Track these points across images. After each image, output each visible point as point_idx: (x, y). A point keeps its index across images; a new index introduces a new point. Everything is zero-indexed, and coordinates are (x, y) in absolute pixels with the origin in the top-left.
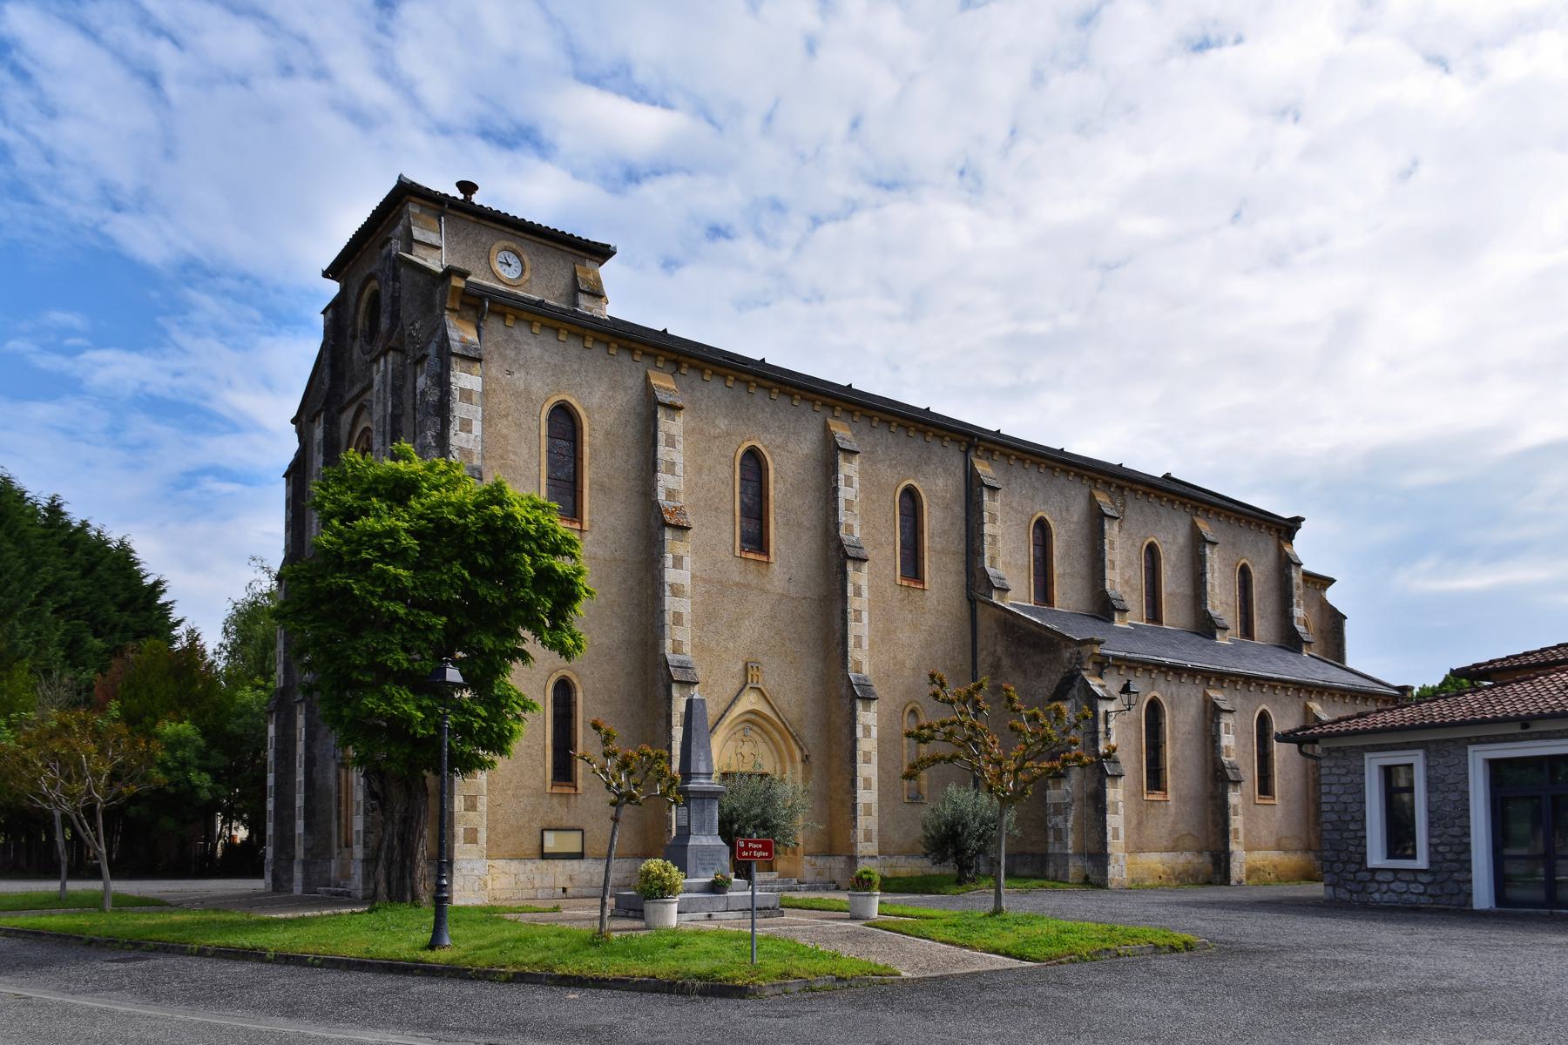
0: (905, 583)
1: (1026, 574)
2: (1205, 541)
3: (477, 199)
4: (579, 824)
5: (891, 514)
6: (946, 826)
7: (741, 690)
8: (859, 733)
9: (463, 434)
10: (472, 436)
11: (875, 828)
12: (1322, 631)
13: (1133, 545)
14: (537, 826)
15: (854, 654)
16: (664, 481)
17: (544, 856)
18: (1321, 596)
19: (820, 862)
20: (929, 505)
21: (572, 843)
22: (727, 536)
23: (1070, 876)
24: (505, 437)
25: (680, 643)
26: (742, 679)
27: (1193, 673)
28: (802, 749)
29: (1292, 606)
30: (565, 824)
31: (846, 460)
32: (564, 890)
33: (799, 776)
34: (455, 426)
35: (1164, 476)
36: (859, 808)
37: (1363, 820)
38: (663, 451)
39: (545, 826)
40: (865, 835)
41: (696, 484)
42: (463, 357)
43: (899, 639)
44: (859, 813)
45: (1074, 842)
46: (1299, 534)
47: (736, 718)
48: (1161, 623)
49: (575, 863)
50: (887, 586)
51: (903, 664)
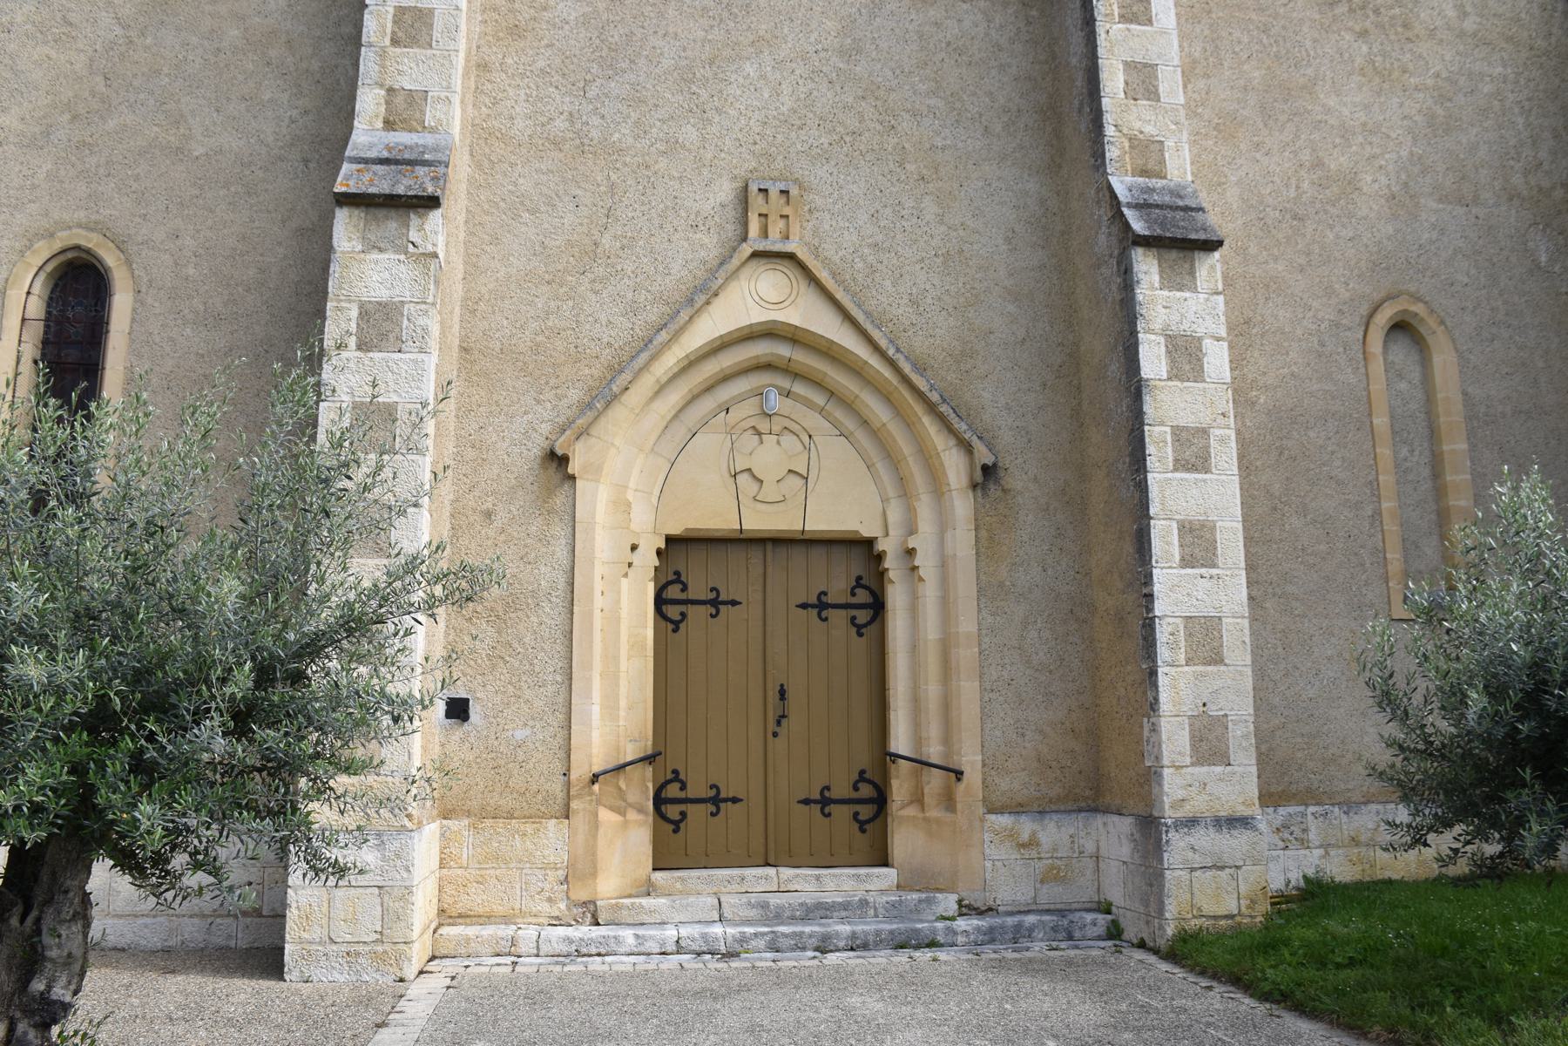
6: (1495, 692)
8: (1153, 361)
11: (1239, 708)
19: (1054, 833)
25: (417, 99)
26: (731, 230)
28: (967, 447)
33: (963, 541)
36: (1162, 634)
40: (1197, 739)
43: (1328, 110)
44: (1163, 653)
47: (692, 363)
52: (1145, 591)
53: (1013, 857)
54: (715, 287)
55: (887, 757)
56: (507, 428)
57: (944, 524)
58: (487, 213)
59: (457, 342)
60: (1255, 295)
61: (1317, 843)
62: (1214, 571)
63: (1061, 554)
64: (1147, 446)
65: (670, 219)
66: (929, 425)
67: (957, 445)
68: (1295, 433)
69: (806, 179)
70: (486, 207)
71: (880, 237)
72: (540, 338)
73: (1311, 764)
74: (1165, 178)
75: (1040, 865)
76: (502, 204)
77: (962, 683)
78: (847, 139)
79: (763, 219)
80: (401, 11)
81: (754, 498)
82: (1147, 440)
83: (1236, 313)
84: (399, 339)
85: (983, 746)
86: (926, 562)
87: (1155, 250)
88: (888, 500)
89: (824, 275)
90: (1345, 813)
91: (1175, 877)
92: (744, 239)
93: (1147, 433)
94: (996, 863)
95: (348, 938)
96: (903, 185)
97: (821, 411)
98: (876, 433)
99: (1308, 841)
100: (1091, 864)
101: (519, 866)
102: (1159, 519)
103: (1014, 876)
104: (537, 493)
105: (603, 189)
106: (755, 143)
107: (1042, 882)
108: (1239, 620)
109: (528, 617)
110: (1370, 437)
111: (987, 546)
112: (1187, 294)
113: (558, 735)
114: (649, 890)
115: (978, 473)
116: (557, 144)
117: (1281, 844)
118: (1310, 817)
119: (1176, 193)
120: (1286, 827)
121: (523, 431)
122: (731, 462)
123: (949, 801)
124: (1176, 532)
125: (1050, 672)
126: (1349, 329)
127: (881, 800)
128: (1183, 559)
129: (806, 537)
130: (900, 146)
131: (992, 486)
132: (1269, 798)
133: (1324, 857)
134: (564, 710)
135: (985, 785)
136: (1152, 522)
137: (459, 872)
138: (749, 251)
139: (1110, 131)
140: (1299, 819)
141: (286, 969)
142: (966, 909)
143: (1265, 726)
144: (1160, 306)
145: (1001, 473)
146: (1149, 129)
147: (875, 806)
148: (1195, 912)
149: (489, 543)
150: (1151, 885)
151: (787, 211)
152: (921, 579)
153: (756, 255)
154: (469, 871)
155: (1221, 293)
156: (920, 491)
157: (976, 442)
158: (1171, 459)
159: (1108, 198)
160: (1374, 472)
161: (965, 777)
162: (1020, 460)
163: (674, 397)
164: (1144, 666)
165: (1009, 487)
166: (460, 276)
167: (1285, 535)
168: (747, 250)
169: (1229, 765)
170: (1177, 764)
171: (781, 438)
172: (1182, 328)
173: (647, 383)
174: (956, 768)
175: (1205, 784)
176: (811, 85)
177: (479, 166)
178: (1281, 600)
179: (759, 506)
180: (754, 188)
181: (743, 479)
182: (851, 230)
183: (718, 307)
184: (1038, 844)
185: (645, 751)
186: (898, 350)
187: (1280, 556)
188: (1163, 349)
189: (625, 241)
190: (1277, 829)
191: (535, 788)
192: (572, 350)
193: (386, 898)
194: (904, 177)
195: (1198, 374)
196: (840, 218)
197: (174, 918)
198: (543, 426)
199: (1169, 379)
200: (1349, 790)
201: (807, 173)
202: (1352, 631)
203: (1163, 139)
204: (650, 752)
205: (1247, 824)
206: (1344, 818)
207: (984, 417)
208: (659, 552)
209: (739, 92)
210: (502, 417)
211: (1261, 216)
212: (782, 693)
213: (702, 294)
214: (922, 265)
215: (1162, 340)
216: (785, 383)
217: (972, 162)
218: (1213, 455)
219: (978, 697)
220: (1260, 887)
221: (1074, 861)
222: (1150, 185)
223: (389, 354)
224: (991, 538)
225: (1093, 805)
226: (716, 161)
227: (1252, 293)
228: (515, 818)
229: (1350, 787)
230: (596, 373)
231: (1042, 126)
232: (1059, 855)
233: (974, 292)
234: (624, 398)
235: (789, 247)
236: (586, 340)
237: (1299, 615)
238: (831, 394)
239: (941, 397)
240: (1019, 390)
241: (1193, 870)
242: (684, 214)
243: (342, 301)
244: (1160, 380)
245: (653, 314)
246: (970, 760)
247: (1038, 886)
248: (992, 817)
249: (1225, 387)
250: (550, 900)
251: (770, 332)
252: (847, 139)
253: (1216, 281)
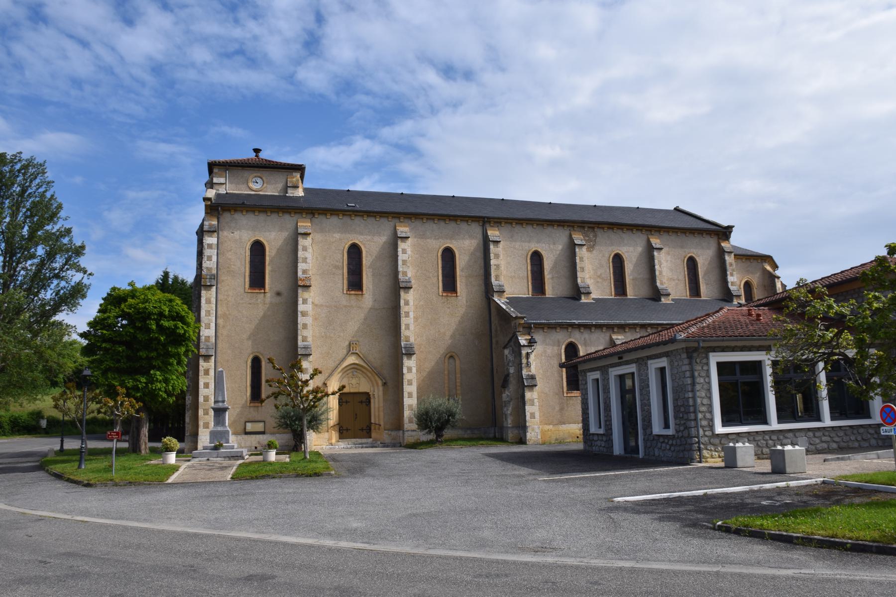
0: (444, 294)
1: (525, 281)
2: (654, 248)
3: (262, 155)
4: (263, 419)
5: (436, 262)
7: (347, 354)
8: (405, 370)
9: (208, 262)
10: (212, 262)
12: (765, 286)
13: (603, 256)
14: (243, 420)
15: (404, 332)
16: (301, 266)
17: (246, 433)
18: (763, 266)
19: (394, 433)
20: (460, 255)
21: (259, 427)
22: (340, 285)
23: (509, 438)
24: (230, 259)
25: (306, 337)
27: (599, 327)
29: (727, 276)
30: (256, 419)
31: (402, 242)
32: (256, 448)
33: (381, 393)
34: (205, 259)
35: (675, 209)
36: (405, 407)
37: (650, 406)
38: (301, 254)
39: (247, 420)
41: (323, 264)
42: (208, 231)
45: (512, 421)
46: (733, 235)
48: (627, 295)
49: (261, 436)
50: (434, 297)
80: (303, 324)
86: (376, 396)
91: (406, 437)
111: (384, 394)
114: (339, 442)
116: (323, 337)
123: (379, 429)
127: (370, 429)
142: (381, 443)
147: (580, 446)
163: (341, 374)
173: (337, 372)
195: (411, 372)
212: (356, 415)
213: (344, 359)
238: (363, 372)
245: (338, 362)
246: (382, 423)
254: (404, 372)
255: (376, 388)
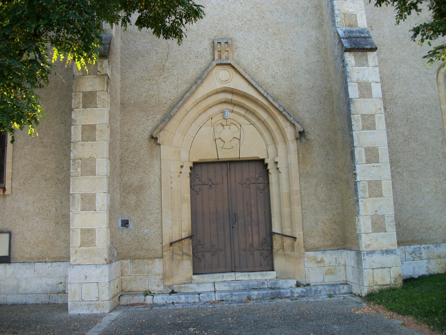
8: (353, 91)
28: (294, 125)
33: (293, 158)
36: (360, 187)
40: (374, 224)
44: (360, 194)
51: (78, 61)
52: (354, 172)
53: (315, 266)
54: (204, 77)
55: (272, 234)
56: (137, 129)
57: (287, 153)
58: (127, 58)
59: (119, 102)
60: (396, 65)
61: (425, 258)
62: (378, 164)
63: (328, 161)
64: (352, 122)
65: (188, 55)
66: (280, 119)
67: (290, 125)
68: (412, 113)
69: (234, 38)
70: (127, 56)
71: (260, 56)
72: (147, 99)
73: (422, 230)
74: (357, 27)
75: (325, 269)
76: (132, 55)
77: (295, 207)
78: (248, 22)
79: (219, 52)
81: (222, 147)
82: (352, 120)
83: (389, 72)
84: (96, 103)
85: (303, 228)
87: (353, 53)
88: (268, 145)
89: (241, 70)
90: (435, 247)
92: (214, 60)
93: (352, 118)
94: (309, 268)
95: (88, 299)
96: (268, 37)
97: (244, 116)
98: (263, 123)
99: (422, 257)
100: (343, 268)
101: (147, 274)
102: (358, 147)
103: (316, 273)
104: (148, 151)
105: (165, 47)
106: (216, 27)
107: (326, 275)
108: (388, 181)
109: (147, 192)
110: (440, 113)
112: (365, 68)
113: (158, 231)
115: (298, 134)
117: (412, 259)
118: (422, 249)
119: (361, 32)
120: (413, 252)
121: (142, 130)
122: (214, 136)
123: (293, 248)
124: (364, 151)
125: (326, 202)
126: (431, 75)
128: (367, 160)
129: (241, 159)
130: (266, 23)
131: (303, 139)
132: (400, 243)
133: (427, 263)
134: (160, 222)
135: (304, 242)
136: (355, 148)
137: (128, 277)
138: (215, 64)
139: (336, 12)
140: (418, 249)
141: (69, 310)
143: (405, 217)
144: (355, 73)
145: (306, 134)
146: (351, 11)
148: (375, 284)
149: (133, 168)
150: (360, 275)
151: (228, 49)
152: (280, 172)
153: (218, 65)
154: (131, 277)
155: (377, 66)
156: (278, 142)
157: (296, 124)
158: (361, 126)
159: (337, 36)
160: (442, 125)
161: (297, 240)
162: (313, 129)
164: (355, 199)
165: (309, 138)
166: (119, 80)
167: (410, 149)
168: (214, 63)
169: (386, 232)
170: (367, 232)
171: (230, 127)
172: (364, 79)
174: (294, 236)
175: (377, 239)
176: (235, 5)
177: (124, 42)
178: (409, 173)
179: (224, 150)
180: (216, 42)
181: (218, 141)
182: (250, 54)
183: (206, 83)
184: (324, 262)
185: (189, 234)
186: (268, 94)
187: (408, 157)
188: (357, 87)
189: (173, 64)
190: (411, 253)
191: (152, 248)
192: (158, 102)
193: (99, 286)
194: (268, 34)
195: (370, 95)
196: (246, 50)
197: (38, 295)
198: (149, 128)
199: (360, 98)
200: (437, 239)
201: (234, 35)
202: (436, 182)
203: (356, 13)
204: (190, 235)
205: (393, 252)
206: (435, 249)
207: (299, 115)
208: (191, 168)
209: (210, 10)
210: (135, 126)
211: (397, 37)
214: (276, 64)
215: (357, 84)
216: (230, 107)
217: (292, 27)
218: (376, 124)
219: (301, 212)
220: (398, 274)
221: (337, 267)
222: (352, 30)
223: (93, 108)
224: (303, 157)
225: (343, 247)
226: (203, 34)
227: (395, 64)
228: (145, 259)
229: (437, 238)
230: (165, 109)
231: (316, 12)
232: (332, 265)
233: (294, 72)
234: (175, 117)
235: (229, 62)
236: (162, 98)
237: (416, 178)
239: (283, 109)
240: (311, 105)
241: (373, 269)
242: (193, 53)
243: (77, 92)
244: (356, 98)
246: (299, 234)
247: (324, 276)
248: (307, 253)
249: (380, 99)
250: (158, 285)
251: (225, 91)
252: (248, 22)
253: (376, 62)
254: (351, 96)
255: (281, 147)
